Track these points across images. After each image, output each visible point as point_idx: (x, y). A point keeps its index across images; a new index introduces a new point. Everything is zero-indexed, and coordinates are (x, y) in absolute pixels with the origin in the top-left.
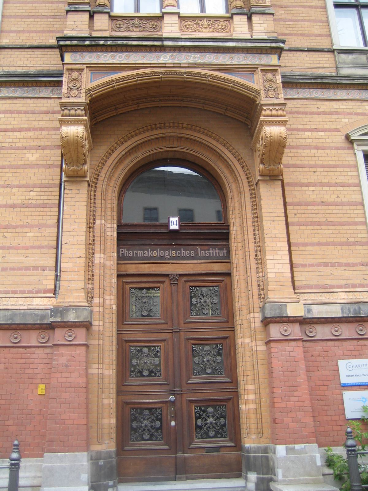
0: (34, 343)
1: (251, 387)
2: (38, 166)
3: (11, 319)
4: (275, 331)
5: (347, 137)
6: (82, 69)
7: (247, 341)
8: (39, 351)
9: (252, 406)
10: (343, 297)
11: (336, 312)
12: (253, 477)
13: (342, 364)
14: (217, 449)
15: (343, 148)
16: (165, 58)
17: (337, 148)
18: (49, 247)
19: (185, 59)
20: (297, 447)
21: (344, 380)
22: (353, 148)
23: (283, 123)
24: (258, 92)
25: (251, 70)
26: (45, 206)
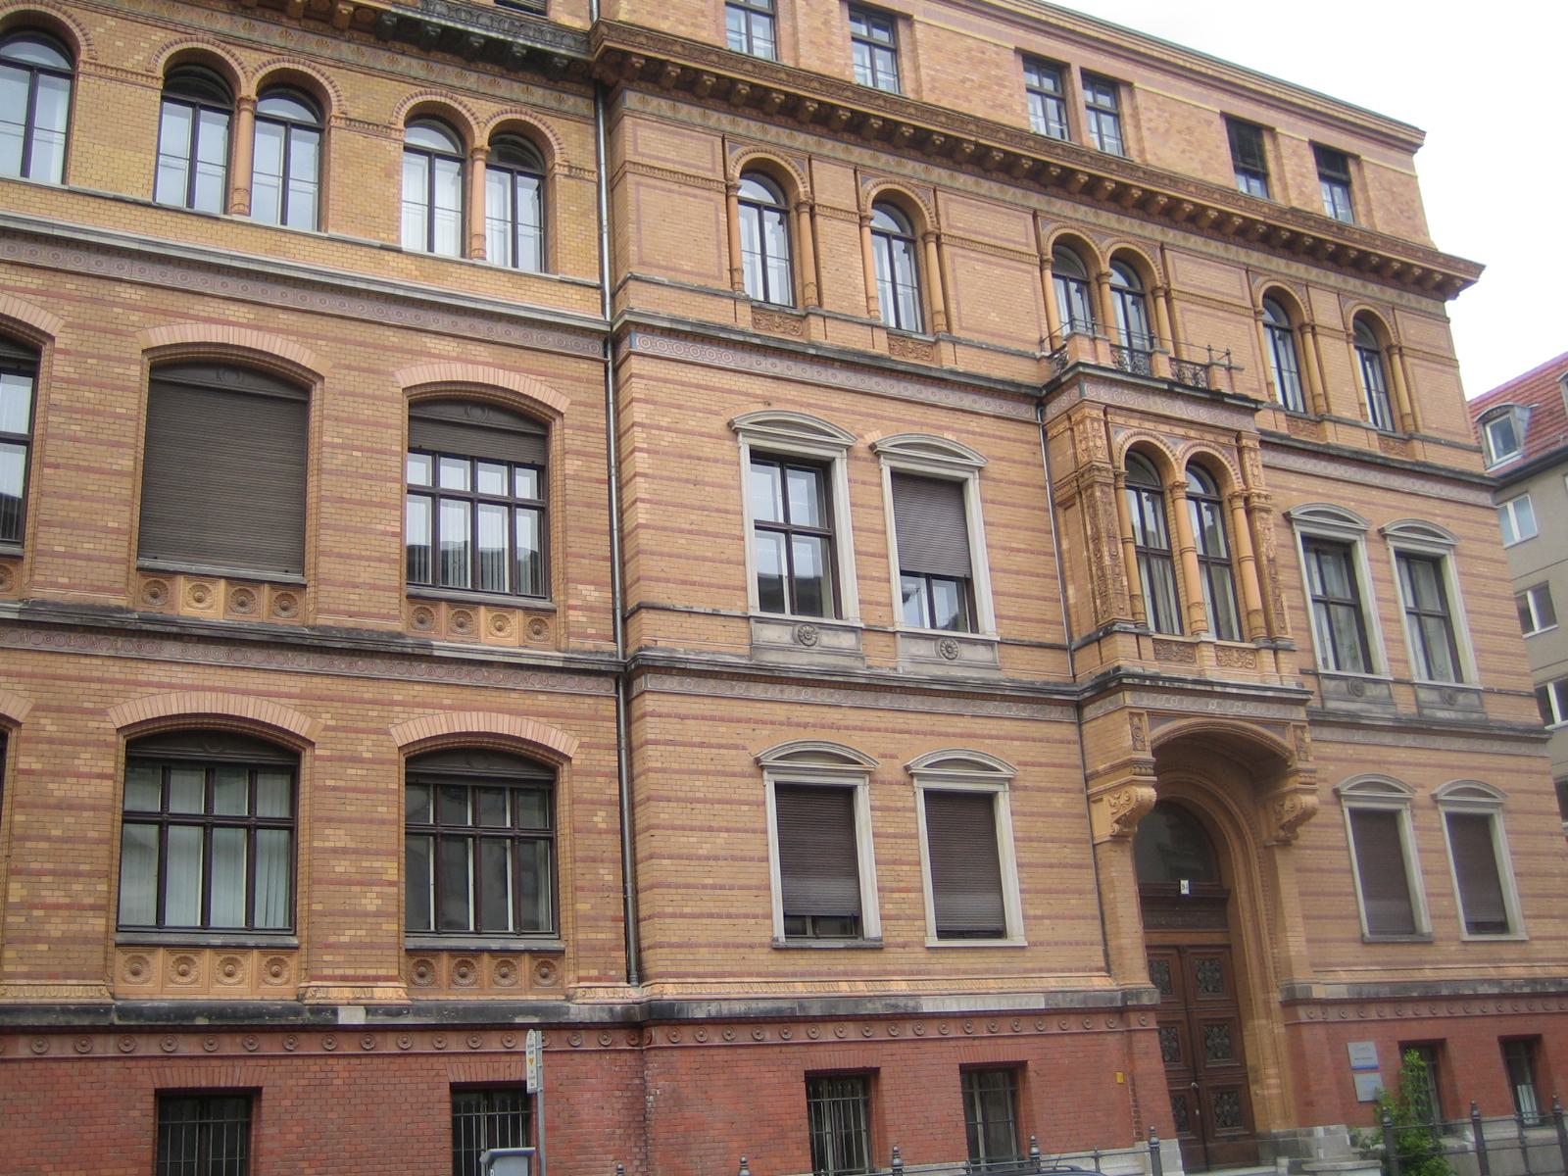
0: (1104, 1028)
1: (1272, 1071)
2: (1065, 816)
3: (1085, 1002)
4: (1303, 1014)
5: (757, 761)
6: (615, 640)
7: (1264, 1022)
8: (1109, 1037)
9: (1275, 1091)
10: (1344, 977)
11: (1342, 993)
12: (1284, 1162)
13: (1351, 1046)
14: (1235, 1138)
15: (751, 776)
16: (1213, 706)
17: (743, 775)
18: (1093, 918)
19: (1235, 709)
20: (1333, 1127)
21: (1354, 1063)
22: (911, 784)
23: (1313, 792)
24: (1291, 753)
25: (1280, 725)
26: (1080, 866)
